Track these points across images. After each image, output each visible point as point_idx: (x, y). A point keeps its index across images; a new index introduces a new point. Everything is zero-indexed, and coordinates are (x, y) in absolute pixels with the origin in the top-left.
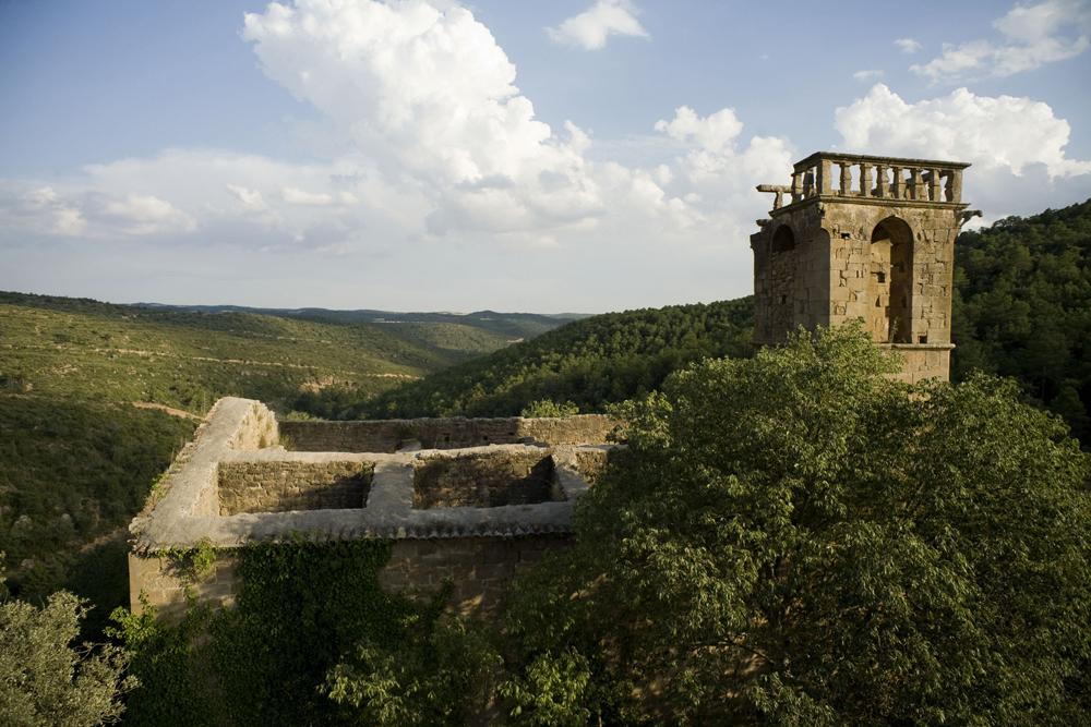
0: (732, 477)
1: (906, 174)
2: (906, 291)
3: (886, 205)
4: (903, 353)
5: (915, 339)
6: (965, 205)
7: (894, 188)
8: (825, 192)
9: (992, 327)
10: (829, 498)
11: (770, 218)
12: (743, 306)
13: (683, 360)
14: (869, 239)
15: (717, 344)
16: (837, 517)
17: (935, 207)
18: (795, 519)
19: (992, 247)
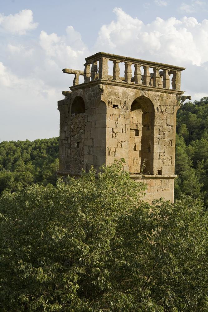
0: (40, 269)
1: (151, 71)
2: (150, 142)
3: (139, 89)
4: (149, 180)
5: (155, 172)
6: (182, 92)
7: (144, 78)
8: (104, 78)
9: (201, 160)
10: (101, 278)
11: (70, 91)
12: (56, 143)
13: (15, 179)
14: (129, 109)
15: (38, 168)
16: (106, 290)
17: (166, 92)
18: (80, 294)
19: (200, 113)
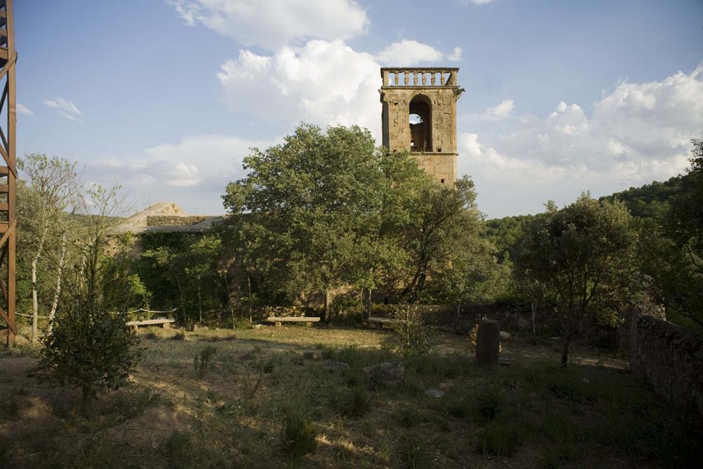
5: (435, 151)
